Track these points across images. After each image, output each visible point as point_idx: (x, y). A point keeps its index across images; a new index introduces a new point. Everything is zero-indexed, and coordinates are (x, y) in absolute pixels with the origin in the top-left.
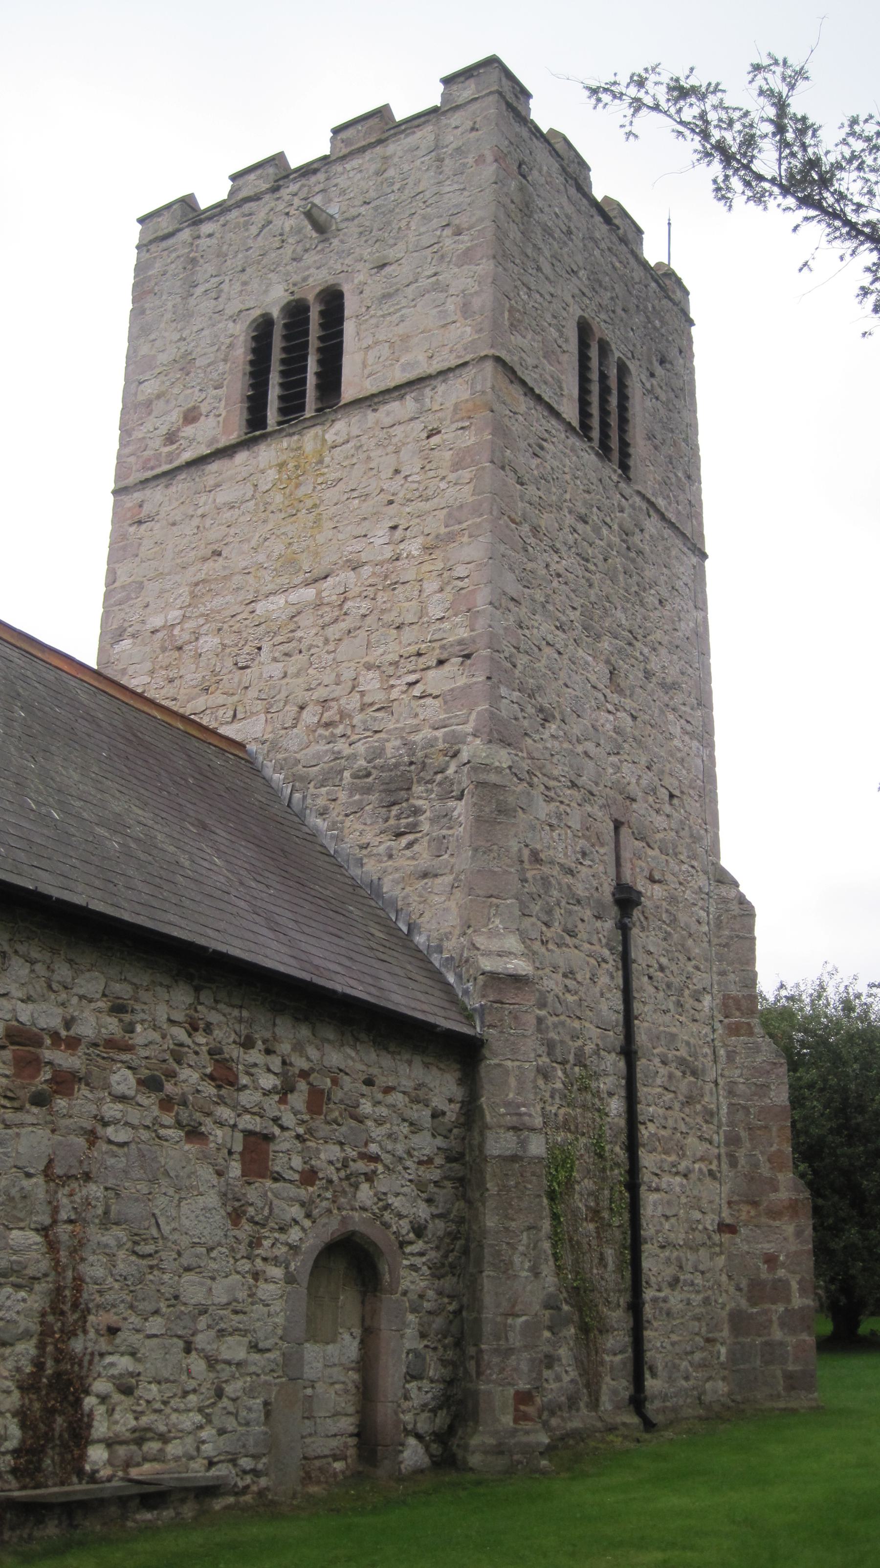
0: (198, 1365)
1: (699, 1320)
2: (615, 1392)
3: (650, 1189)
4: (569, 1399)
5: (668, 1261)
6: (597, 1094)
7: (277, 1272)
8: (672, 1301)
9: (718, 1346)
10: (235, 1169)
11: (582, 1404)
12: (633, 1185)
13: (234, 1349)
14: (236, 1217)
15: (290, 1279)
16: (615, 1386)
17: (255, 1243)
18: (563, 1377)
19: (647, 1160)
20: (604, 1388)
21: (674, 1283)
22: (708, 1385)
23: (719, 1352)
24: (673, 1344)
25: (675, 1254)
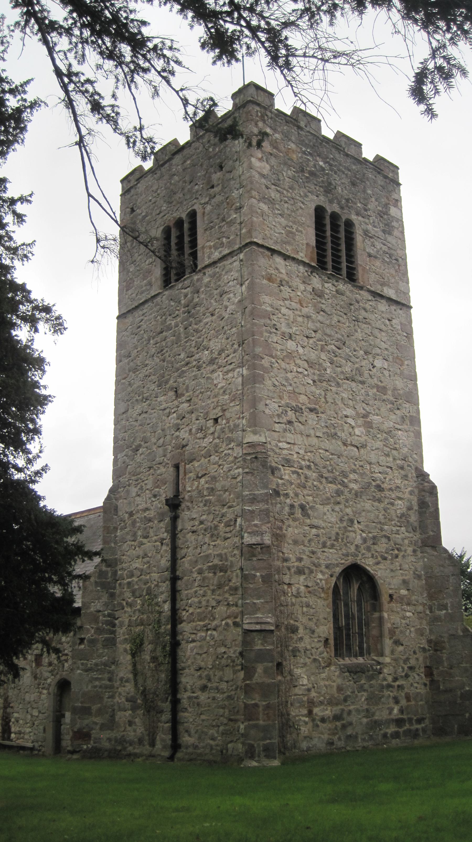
0: (29, 717)
1: (223, 708)
2: (163, 740)
3: (188, 642)
4: (139, 740)
5: (200, 677)
6: (157, 604)
7: (45, 691)
8: (202, 698)
9: (240, 723)
10: (34, 665)
11: (146, 743)
12: (175, 644)
13: (35, 713)
14: (35, 677)
15: (49, 693)
16: (163, 737)
17: (39, 684)
18: (139, 729)
19: (185, 628)
20: (158, 737)
21: (204, 688)
22: (229, 745)
23: (239, 727)
24: (203, 720)
25: (206, 673)
